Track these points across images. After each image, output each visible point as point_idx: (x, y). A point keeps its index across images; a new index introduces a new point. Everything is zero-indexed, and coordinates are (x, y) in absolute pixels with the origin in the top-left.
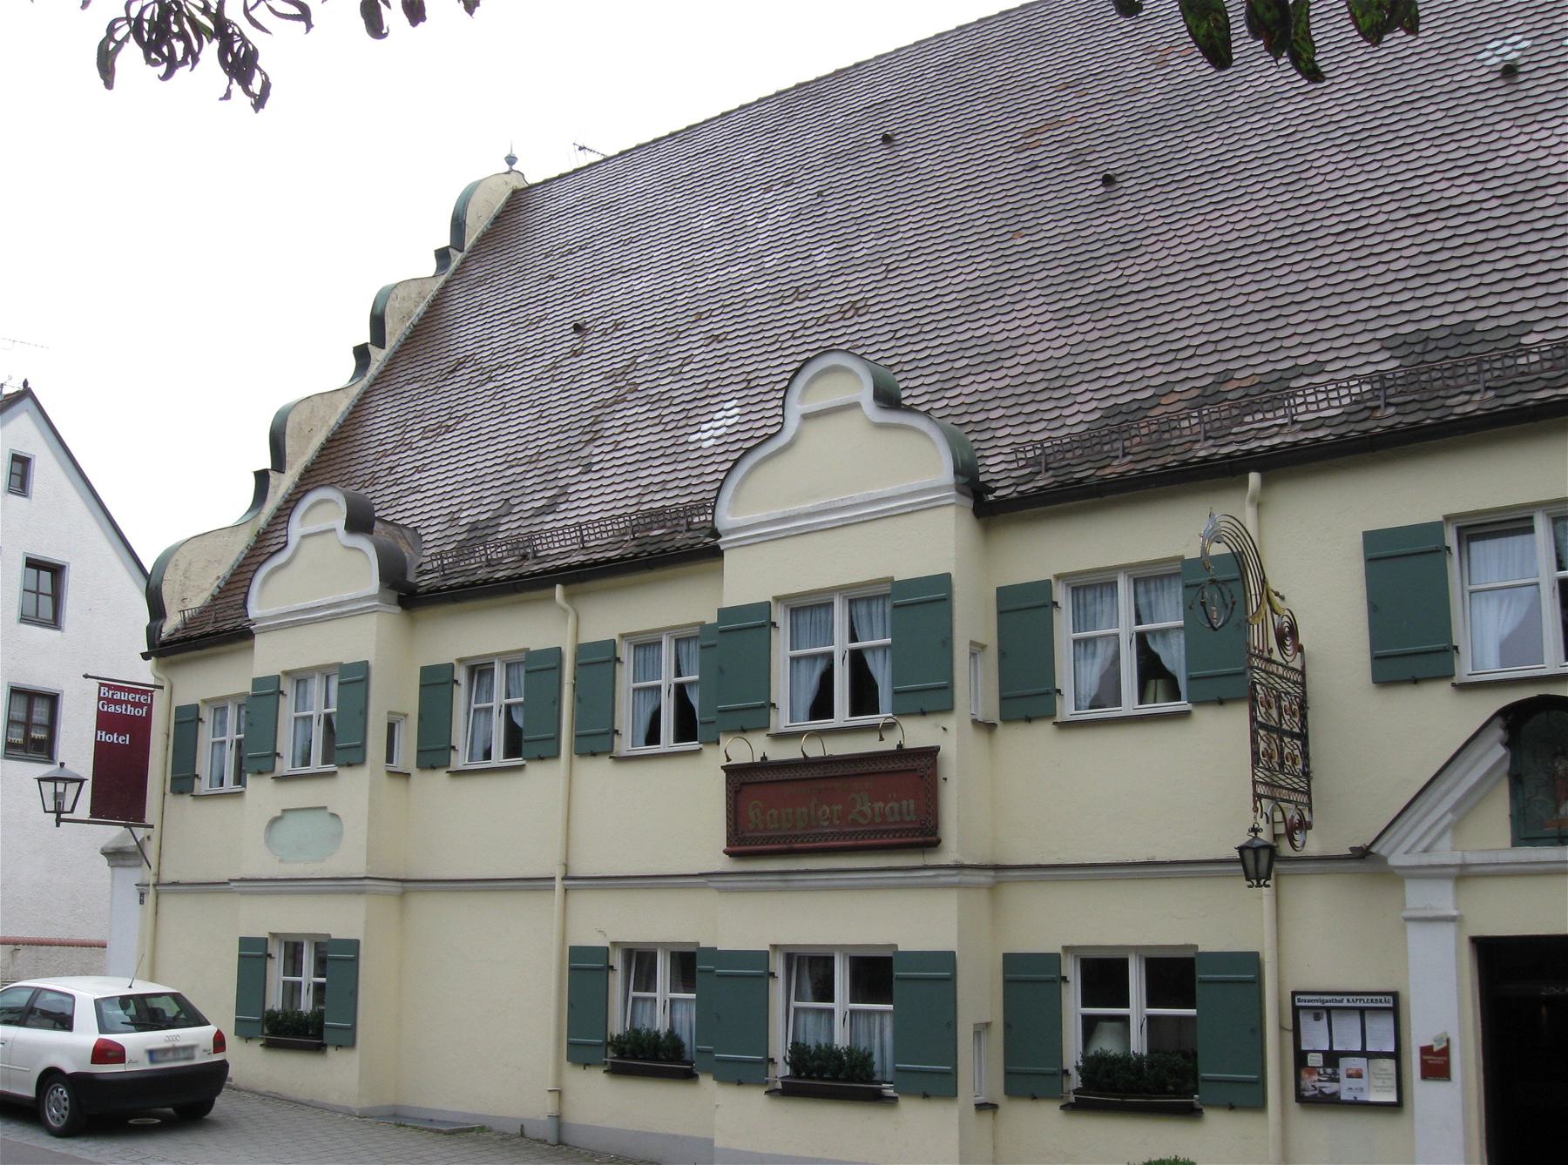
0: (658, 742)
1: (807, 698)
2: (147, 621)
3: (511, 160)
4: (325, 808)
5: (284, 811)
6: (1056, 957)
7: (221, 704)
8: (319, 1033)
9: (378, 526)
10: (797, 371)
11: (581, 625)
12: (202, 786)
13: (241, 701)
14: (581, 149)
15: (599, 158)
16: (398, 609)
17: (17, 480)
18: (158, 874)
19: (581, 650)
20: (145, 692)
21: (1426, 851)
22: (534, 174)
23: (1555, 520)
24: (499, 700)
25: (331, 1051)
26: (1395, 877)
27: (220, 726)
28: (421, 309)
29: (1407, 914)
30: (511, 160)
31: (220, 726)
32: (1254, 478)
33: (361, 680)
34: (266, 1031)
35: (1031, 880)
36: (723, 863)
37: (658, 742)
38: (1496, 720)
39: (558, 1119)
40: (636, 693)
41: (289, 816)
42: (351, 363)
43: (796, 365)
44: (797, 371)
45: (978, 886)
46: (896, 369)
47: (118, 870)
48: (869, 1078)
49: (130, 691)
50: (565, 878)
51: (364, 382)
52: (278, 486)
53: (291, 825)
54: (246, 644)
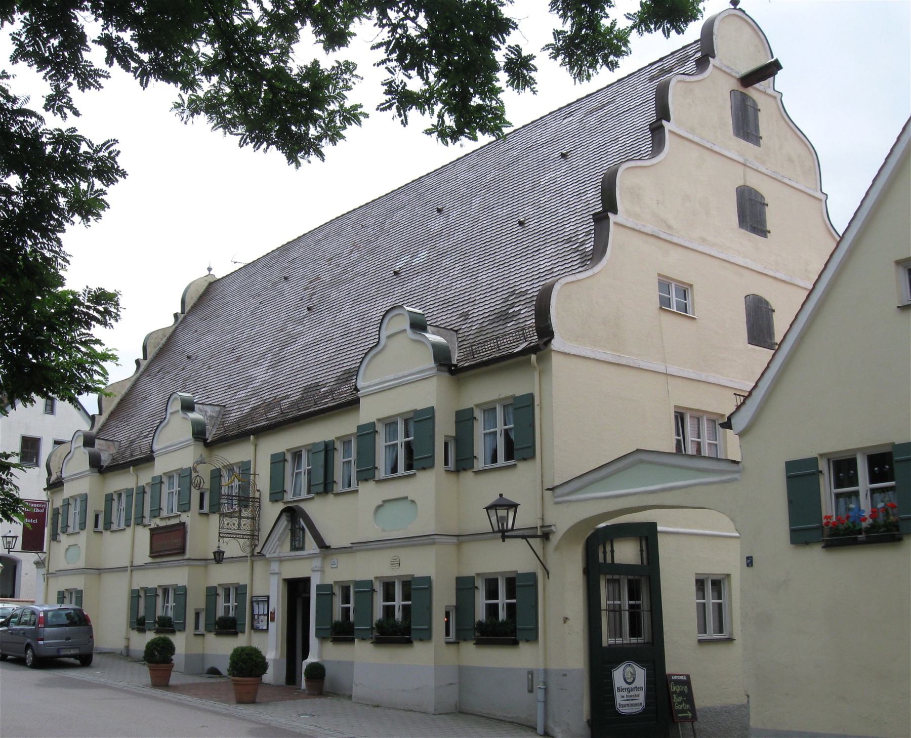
0: (496, 462)
1: (389, 468)
2: (47, 476)
3: (210, 269)
4: (407, 498)
5: (69, 546)
6: (473, 577)
7: (347, 439)
8: (514, 631)
9: (429, 327)
11: (257, 449)
12: (338, 488)
13: (240, 465)
14: (235, 263)
15: (242, 265)
16: (98, 474)
17: (49, 407)
18: (48, 570)
19: (138, 488)
20: (43, 503)
21: (274, 552)
22: (219, 274)
25: (521, 645)
26: (269, 561)
27: (347, 453)
28: (165, 340)
30: (210, 269)
33: (430, 418)
34: (217, 628)
35: (341, 553)
36: (149, 560)
37: (496, 462)
39: (127, 647)
40: (345, 465)
41: (387, 505)
42: (135, 366)
45: (199, 566)
46: (426, 316)
47: (39, 569)
48: (171, 626)
49: (37, 503)
50: (132, 566)
51: (138, 374)
52: (99, 420)
53: (389, 508)
54: (148, 464)
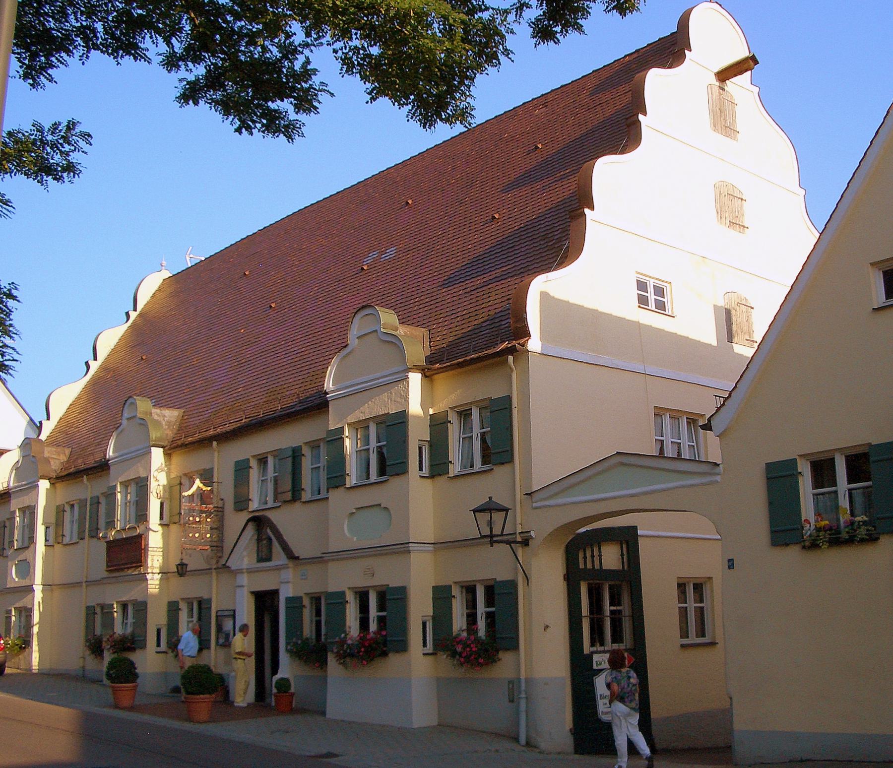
10: (124, 404)
23: (275, 456)
24: (271, 473)
25: (391, 655)
29: (237, 585)
31: (316, 458)
32: (215, 443)
36: (106, 574)
38: (250, 523)
43: (126, 399)
44: (124, 404)
